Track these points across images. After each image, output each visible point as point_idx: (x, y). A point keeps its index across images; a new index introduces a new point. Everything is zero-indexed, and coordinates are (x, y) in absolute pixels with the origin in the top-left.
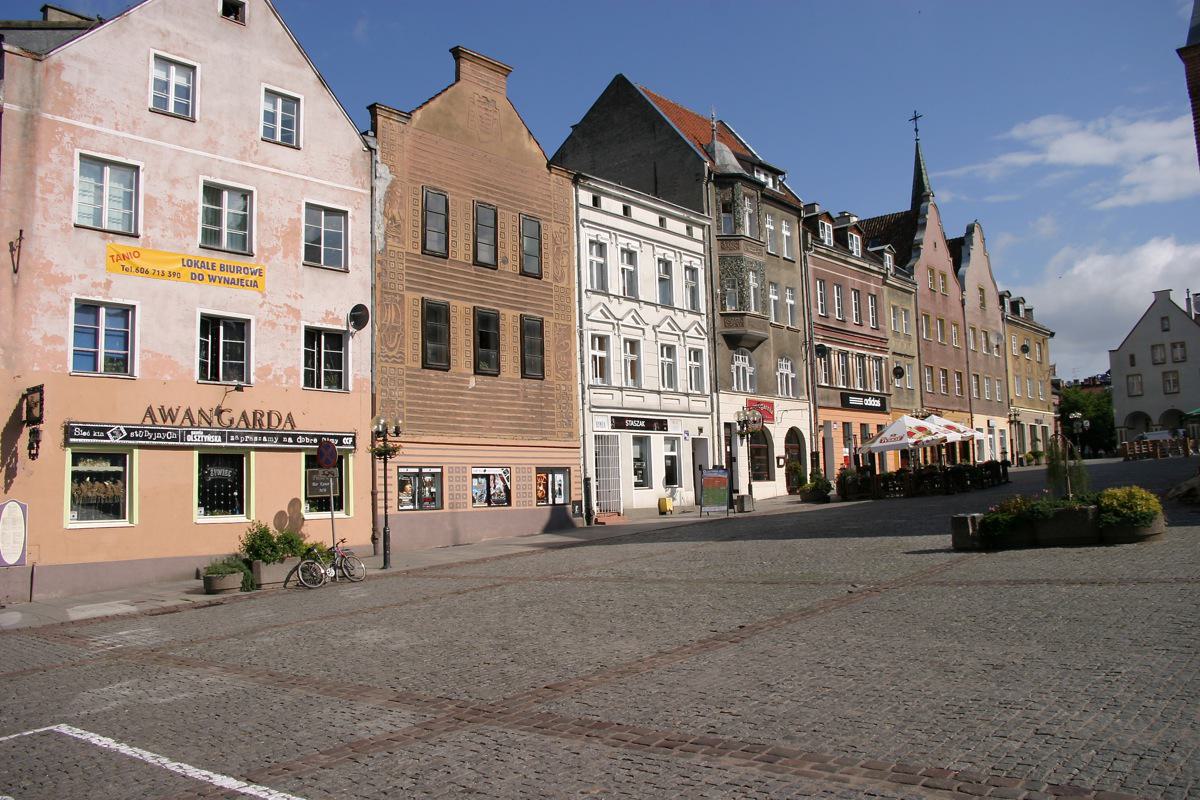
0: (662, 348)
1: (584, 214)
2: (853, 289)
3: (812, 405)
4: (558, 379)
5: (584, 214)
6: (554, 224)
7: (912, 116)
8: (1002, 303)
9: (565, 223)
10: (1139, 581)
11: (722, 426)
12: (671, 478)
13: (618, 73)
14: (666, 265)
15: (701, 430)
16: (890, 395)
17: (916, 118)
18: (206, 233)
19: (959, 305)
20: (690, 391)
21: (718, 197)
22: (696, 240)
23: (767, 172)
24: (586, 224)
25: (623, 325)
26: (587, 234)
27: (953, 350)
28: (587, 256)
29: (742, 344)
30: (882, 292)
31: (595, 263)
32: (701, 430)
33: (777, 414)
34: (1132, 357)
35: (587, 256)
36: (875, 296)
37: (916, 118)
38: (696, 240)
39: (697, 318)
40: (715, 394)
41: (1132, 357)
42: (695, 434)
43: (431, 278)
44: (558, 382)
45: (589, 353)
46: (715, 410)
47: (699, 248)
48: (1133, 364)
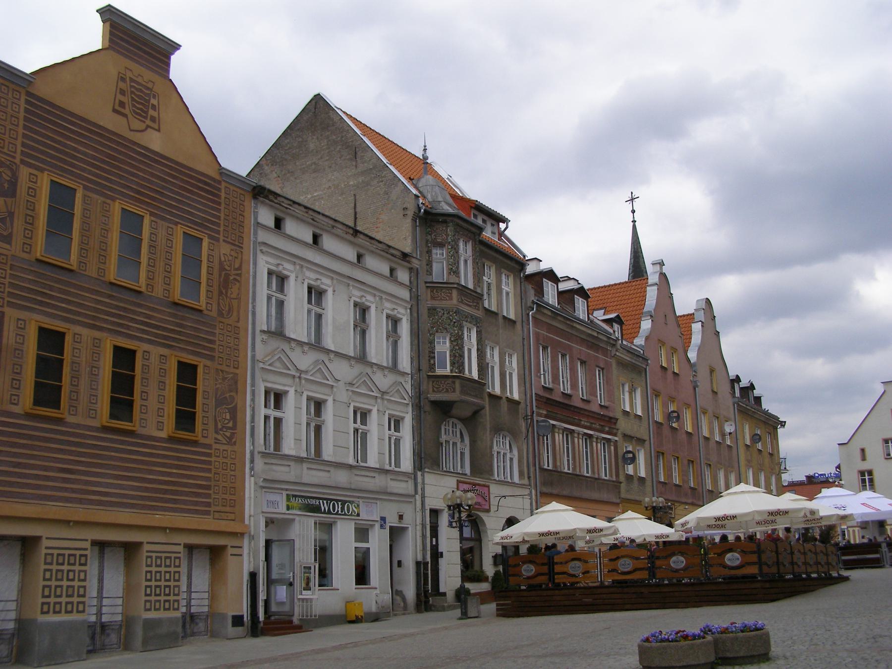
0: (355, 412)
1: (263, 236)
2: (579, 359)
3: (533, 492)
4: (217, 441)
5: (263, 236)
6: (222, 243)
7: (628, 197)
8: (733, 388)
9: (238, 245)
10: (603, 604)
11: (428, 512)
12: (362, 576)
13: (316, 93)
14: (363, 310)
15: (401, 517)
16: (621, 483)
17: (632, 200)
18: (114, 401)
19: (692, 391)
20: (387, 467)
21: (429, 237)
22: (401, 284)
23: (485, 218)
24: (264, 249)
25: (306, 379)
26: (263, 264)
27: (684, 436)
28: (263, 289)
29: (458, 378)
30: (611, 365)
31: (274, 299)
32: (401, 517)
33: (494, 501)
34: (863, 450)
35: (263, 289)
36: (603, 369)
37: (632, 200)
38: (401, 284)
39: (401, 379)
40: (419, 473)
41: (863, 450)
42: (392, 521)
43: (253, 428)
44: (218, 446)
45: (262, 411)
46: (419, 490)
47: (405, 294)
48: (864, 458)
